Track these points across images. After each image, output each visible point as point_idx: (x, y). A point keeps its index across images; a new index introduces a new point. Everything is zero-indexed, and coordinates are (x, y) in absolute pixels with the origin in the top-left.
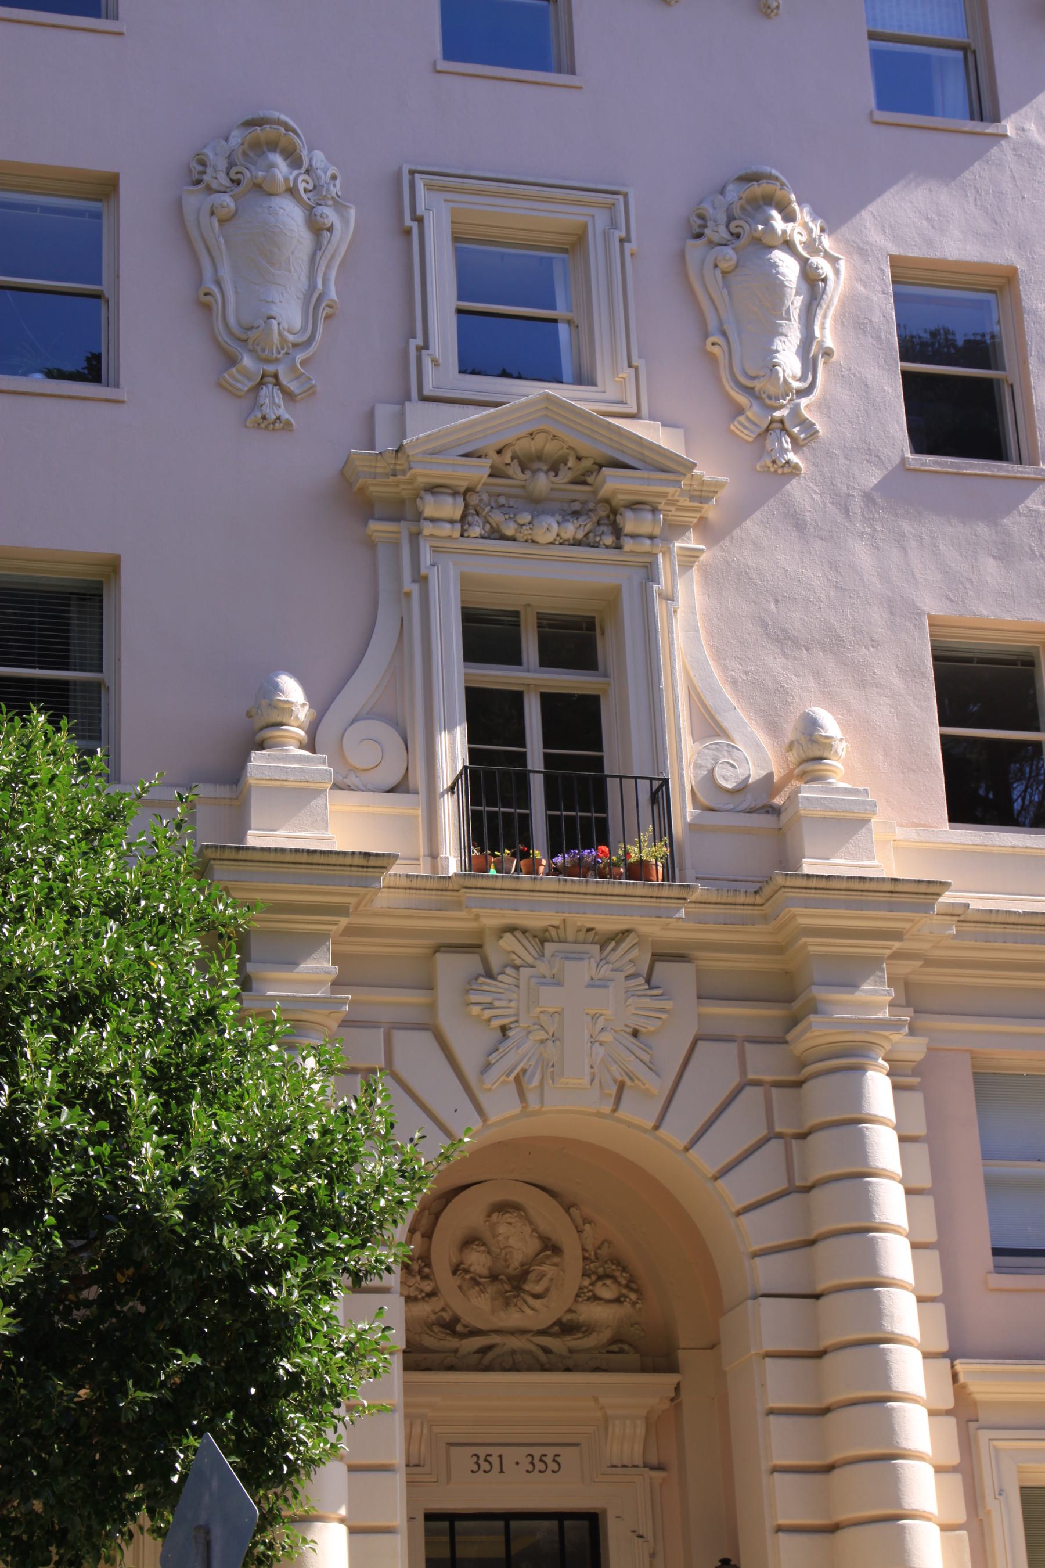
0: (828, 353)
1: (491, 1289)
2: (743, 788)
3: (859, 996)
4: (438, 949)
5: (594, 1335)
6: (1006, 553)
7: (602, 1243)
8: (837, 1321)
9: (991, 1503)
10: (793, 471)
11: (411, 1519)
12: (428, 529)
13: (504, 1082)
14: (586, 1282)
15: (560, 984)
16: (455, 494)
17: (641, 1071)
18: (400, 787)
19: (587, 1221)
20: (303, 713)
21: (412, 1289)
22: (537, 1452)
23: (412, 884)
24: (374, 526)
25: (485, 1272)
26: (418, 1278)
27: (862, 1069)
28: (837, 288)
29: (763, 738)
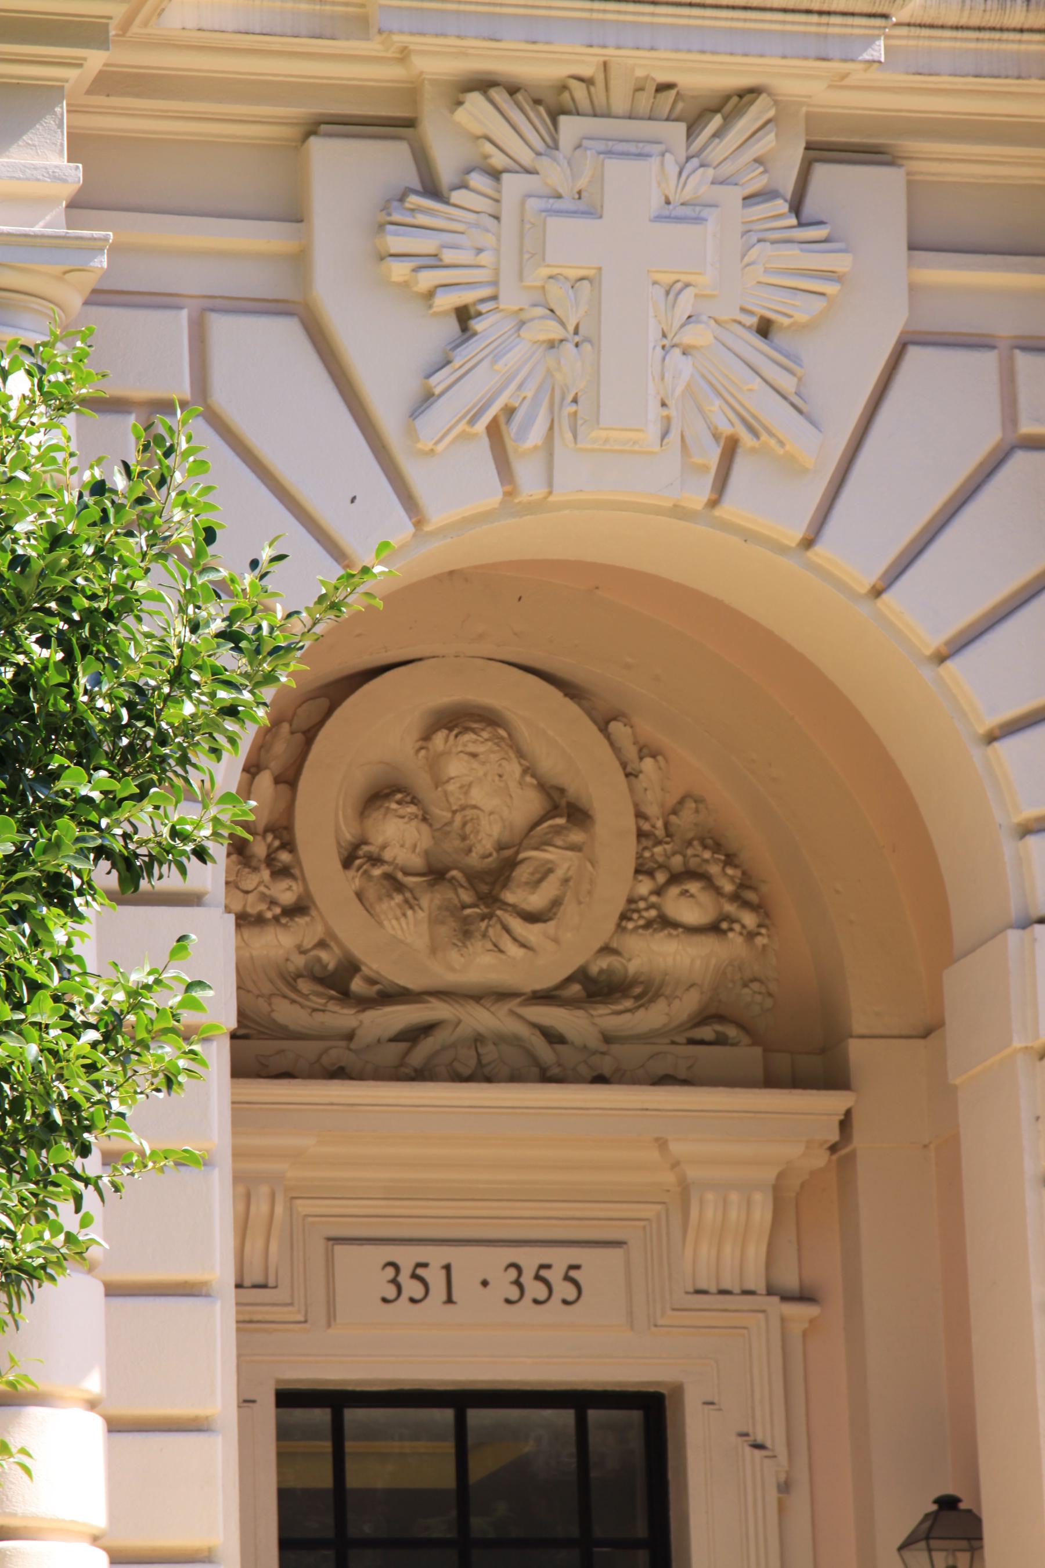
1: (430, 900)
4: (314, 127)
5: (661, 1005)
7: (681, 802)
13: (464, 436)
14: (645, 887)
15: (593, 212)
17: (776, 414)
19: (647, 751)
21: (251, 897)
22: (530, 1259)
25: (416, 861)
26: (266, 874)
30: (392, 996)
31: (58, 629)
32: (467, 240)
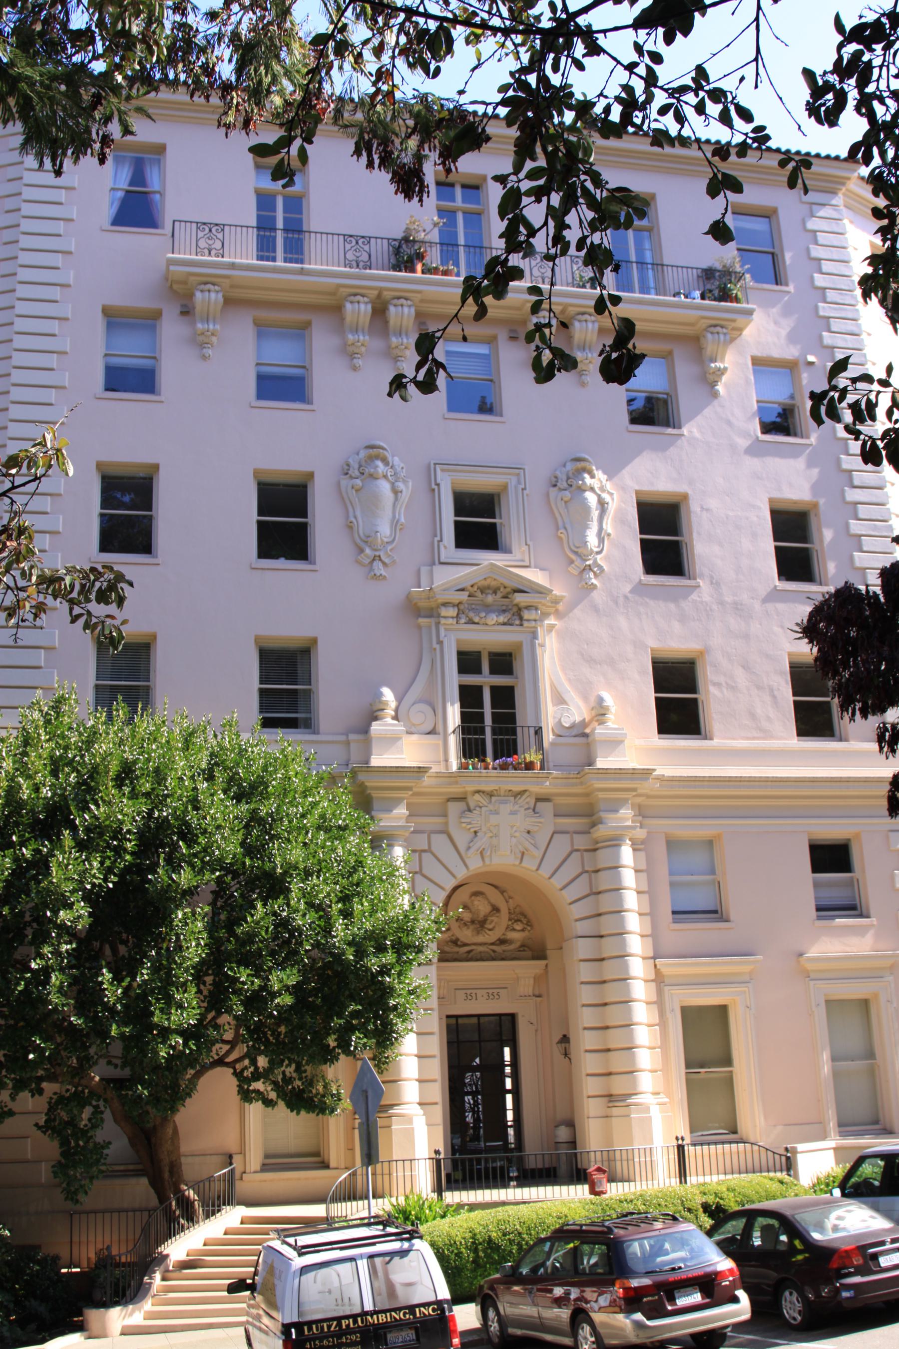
0: (609, 535)
1: (472, 927)
2: (573, 726)
3: (619, 815)
4: (448, 800)
6: (683, 618)
8: (608, 947)
9: (669, 1015)
10: (594, 587)
11: (440, 1019)
12: (443, 621)
16: (454, 606)
17: (531, 848)
18: (432, 732)
19: (511, 898)
20: (393, 705)
22: (490, 991)
23: (439, 775)
24: (421, 620)
27: (619, 846)
28: (612, 508)
29: (581, 703)
30: (465, 945)
31: (870, 61)
32: (476, 820)
